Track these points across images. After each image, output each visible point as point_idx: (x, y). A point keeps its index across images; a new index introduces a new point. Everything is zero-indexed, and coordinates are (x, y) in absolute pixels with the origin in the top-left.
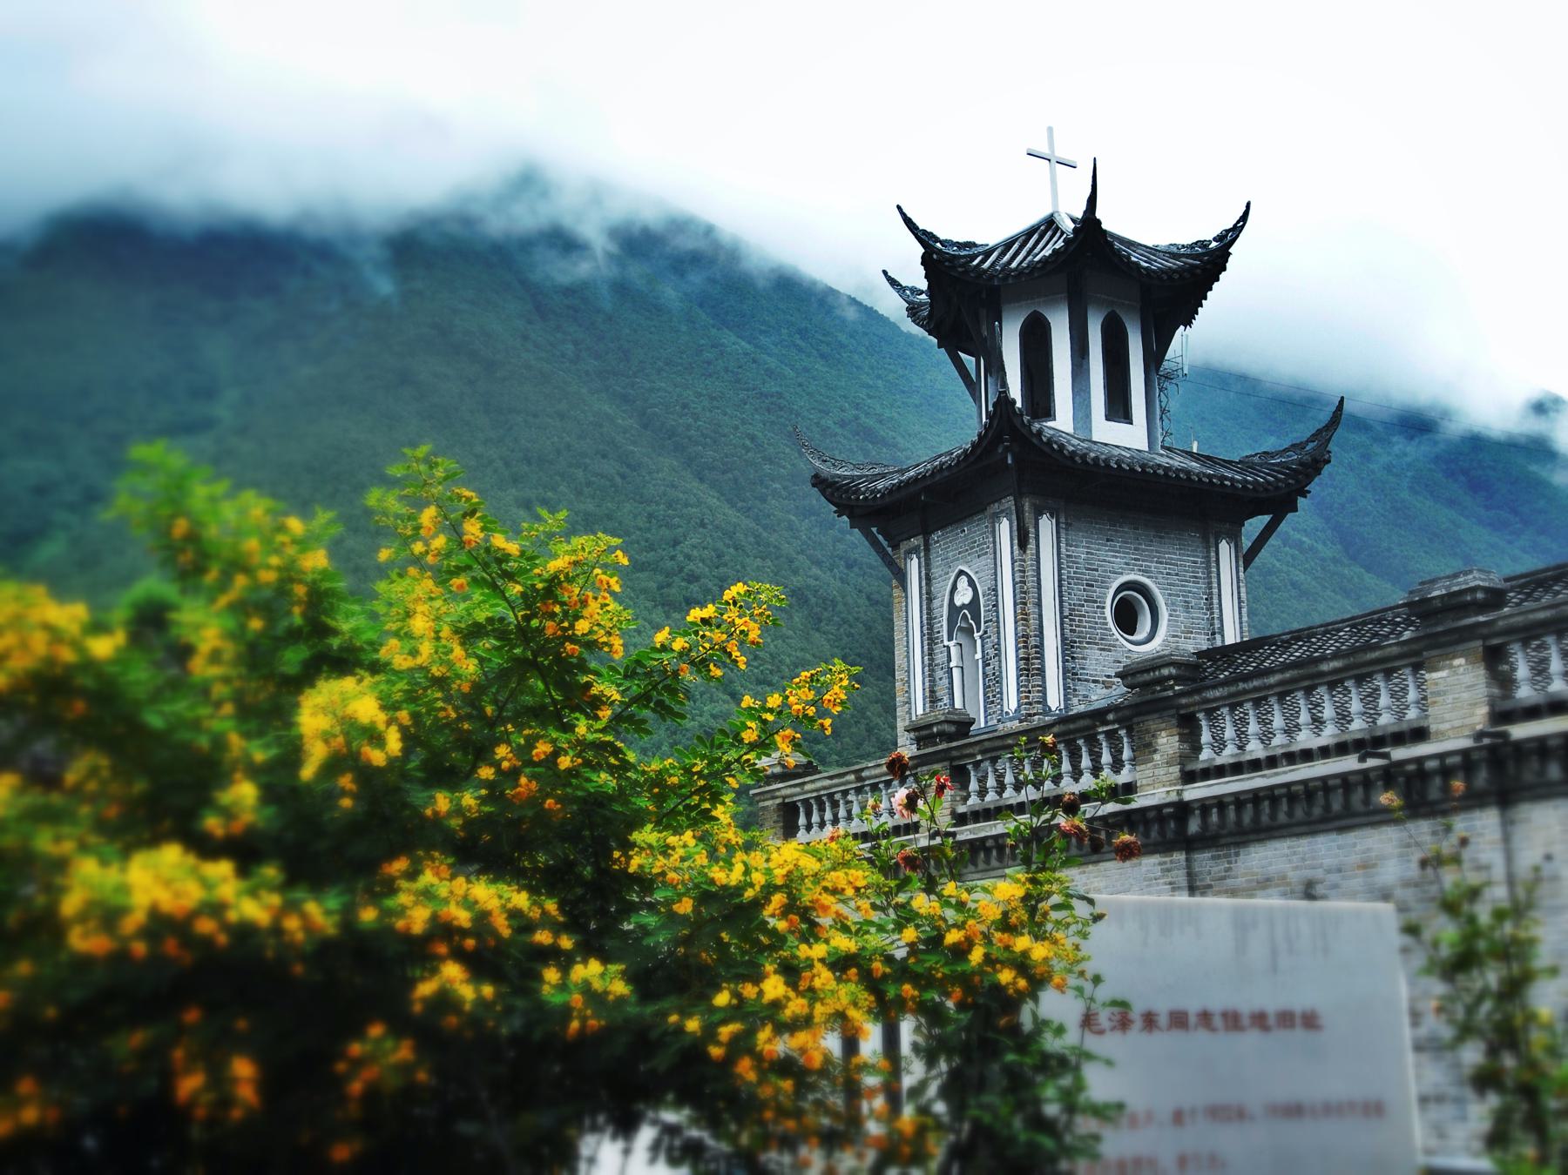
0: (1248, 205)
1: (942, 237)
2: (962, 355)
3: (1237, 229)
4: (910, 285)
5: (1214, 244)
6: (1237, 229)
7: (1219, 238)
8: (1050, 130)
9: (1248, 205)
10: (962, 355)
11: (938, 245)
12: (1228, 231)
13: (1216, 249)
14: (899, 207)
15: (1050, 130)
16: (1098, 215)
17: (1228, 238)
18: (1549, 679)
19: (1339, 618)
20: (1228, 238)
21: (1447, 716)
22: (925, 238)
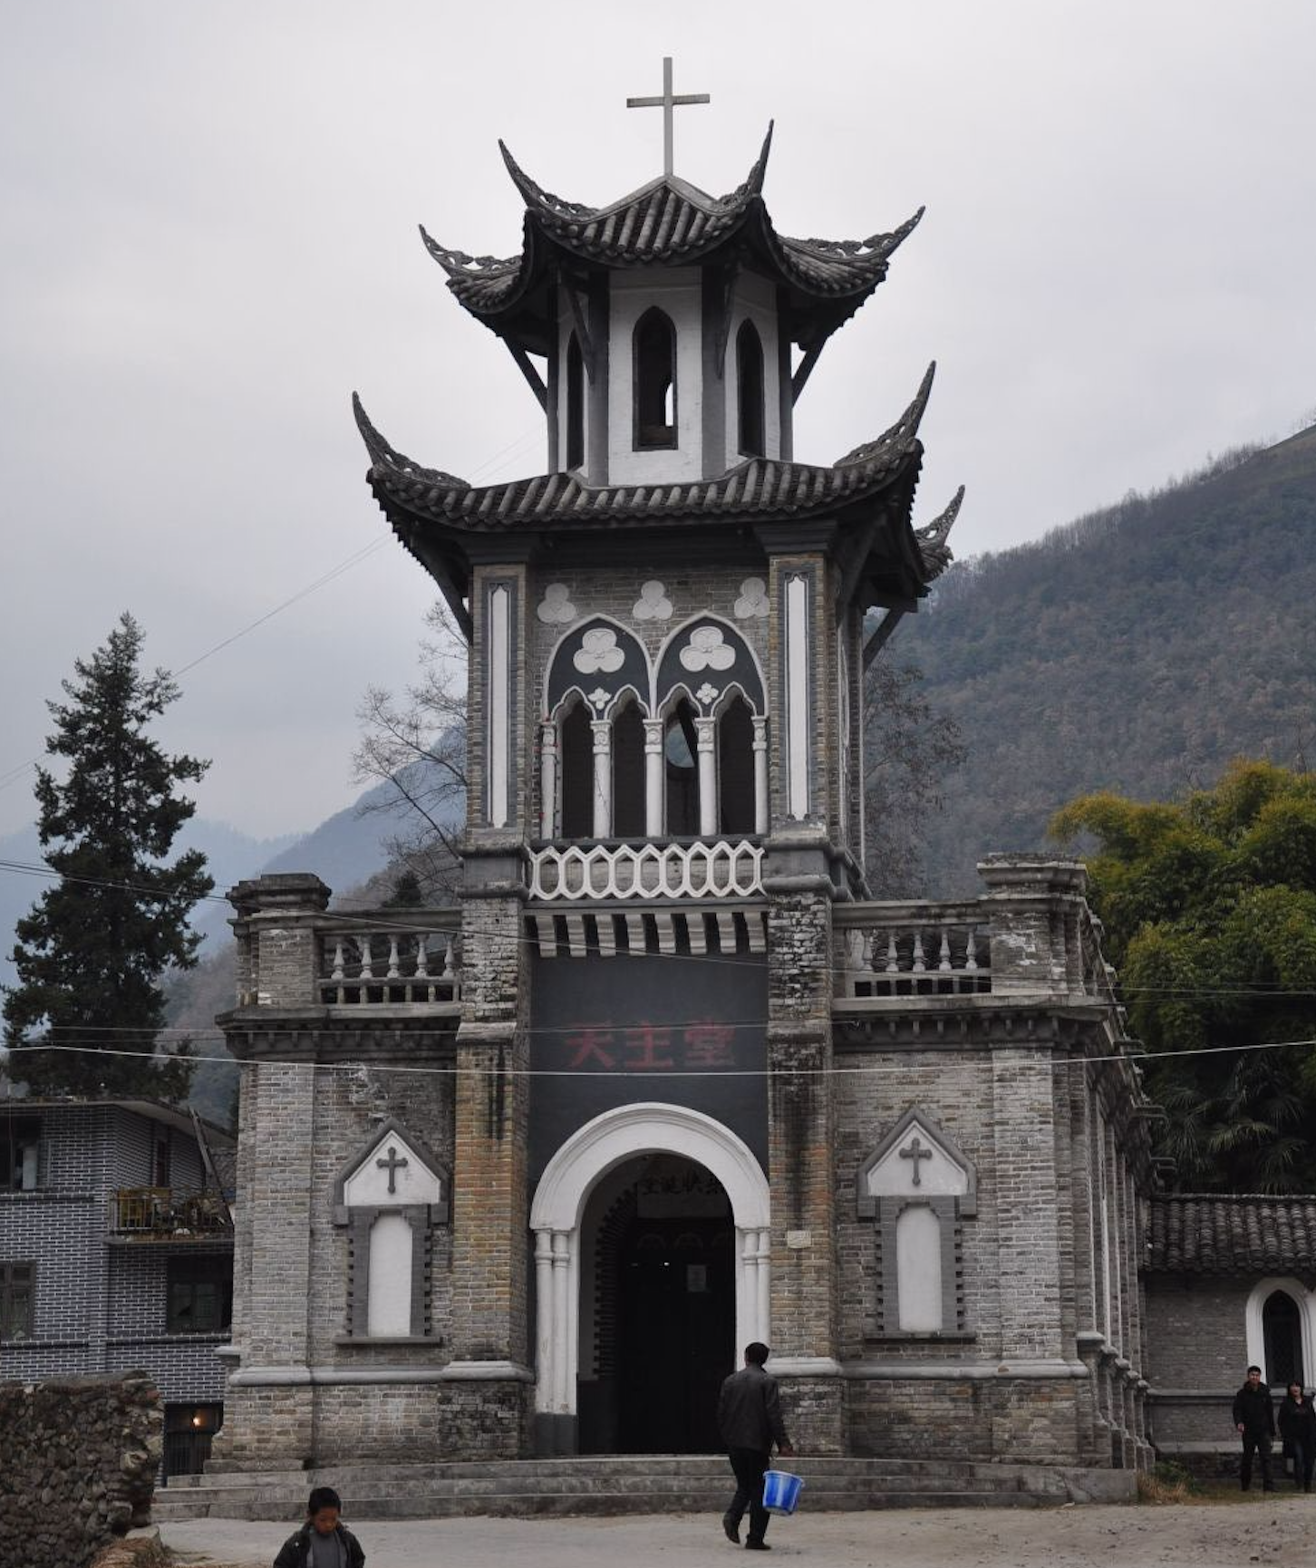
0: (921, 211)
1: (546, 191)
2: (794, 373)
3: (903, 232)
4: (841, 241)
5: (864, 251)
6: (903, 232)
7: (872, 242)
8: (631, 103)
9: (921, 211)
10: (794, 373)
11: (542, 198)
12: (887, 236)
13: (866, 259)
14: (772, 122)
15: (631, 103)
16: (766, 194)
17: (886, 244)
18: (415, 967)
19: (360, 909)
20: (886, 244)
21: (1016, 1311)
22: (526, 186)
